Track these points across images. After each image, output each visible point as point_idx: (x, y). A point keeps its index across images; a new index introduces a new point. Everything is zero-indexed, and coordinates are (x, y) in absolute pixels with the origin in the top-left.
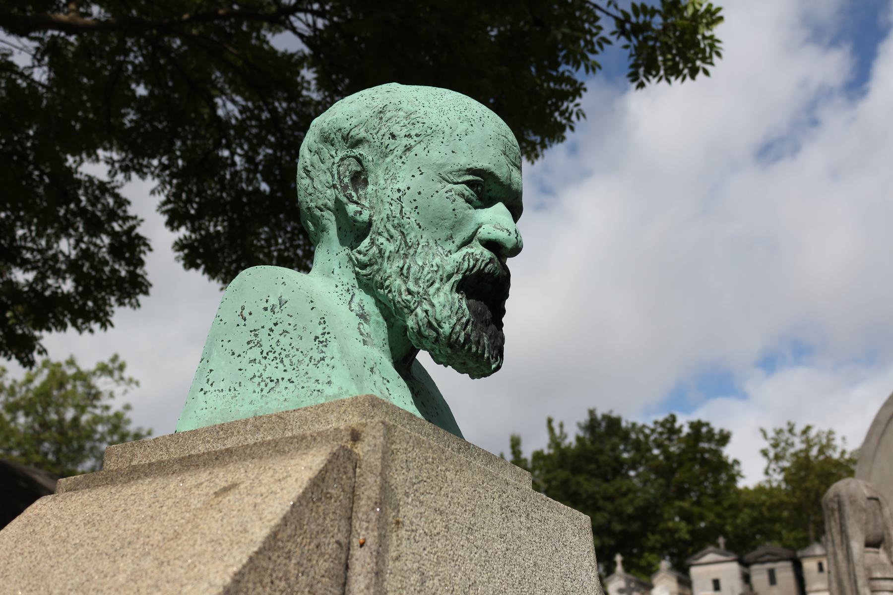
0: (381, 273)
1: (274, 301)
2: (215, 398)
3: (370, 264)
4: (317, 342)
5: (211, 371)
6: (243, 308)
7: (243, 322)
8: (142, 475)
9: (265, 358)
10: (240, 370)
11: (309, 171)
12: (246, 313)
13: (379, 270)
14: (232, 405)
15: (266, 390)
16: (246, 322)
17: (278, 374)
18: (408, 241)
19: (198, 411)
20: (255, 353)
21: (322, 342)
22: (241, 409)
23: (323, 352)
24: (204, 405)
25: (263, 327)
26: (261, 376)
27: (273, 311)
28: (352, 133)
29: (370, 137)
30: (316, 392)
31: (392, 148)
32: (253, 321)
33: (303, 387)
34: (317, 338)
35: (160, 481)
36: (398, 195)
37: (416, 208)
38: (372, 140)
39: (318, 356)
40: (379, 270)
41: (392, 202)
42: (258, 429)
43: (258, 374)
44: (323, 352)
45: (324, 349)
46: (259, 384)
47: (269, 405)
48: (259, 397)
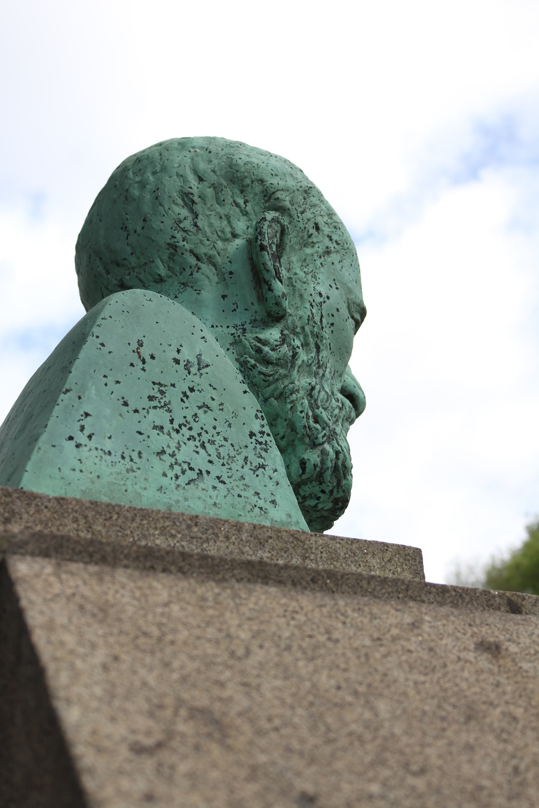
0: (286, 382)
1: (187, 355)
2: (97, 460)
3: (277, 363)
4: (253, 440)
5: (87, 415)
6: (140, 344)
7: (141, 365)
8: (159, 567)
9: (178, 432)
10: (140, 433)
11: (193, 202)
12: (145, 352)
13: (286, 376)
14: (129, 483)
15: (183, 480)
16: (146, 366)
17: (200, 462)
18: (320, 358)
19: (66, 471)
20: (160, 417)
21: (260, 443)
22: (144, 493)
23: (261, 457)
24: (78, 466)
25: (173, 385)
26: (173, 455)
27: (187, 367)
28: (278, 195)
29: (293, 212)
30: (257, 510)
31: (315, 240)
32: (158, 370)
33: (239, 496)
34: (252, 435)
35: (210, 590)
36: (318, 299)
37: (332, 324)
38: (296, 217)
39: (257, 461)
40: (286, 376)
41: (314, 304)
42: (261, 544)
43: (169, 451)
44: (261, 457)
45: (263, 454)
46: (171, 466)
47: (190, 503)
48: (173, 486)
